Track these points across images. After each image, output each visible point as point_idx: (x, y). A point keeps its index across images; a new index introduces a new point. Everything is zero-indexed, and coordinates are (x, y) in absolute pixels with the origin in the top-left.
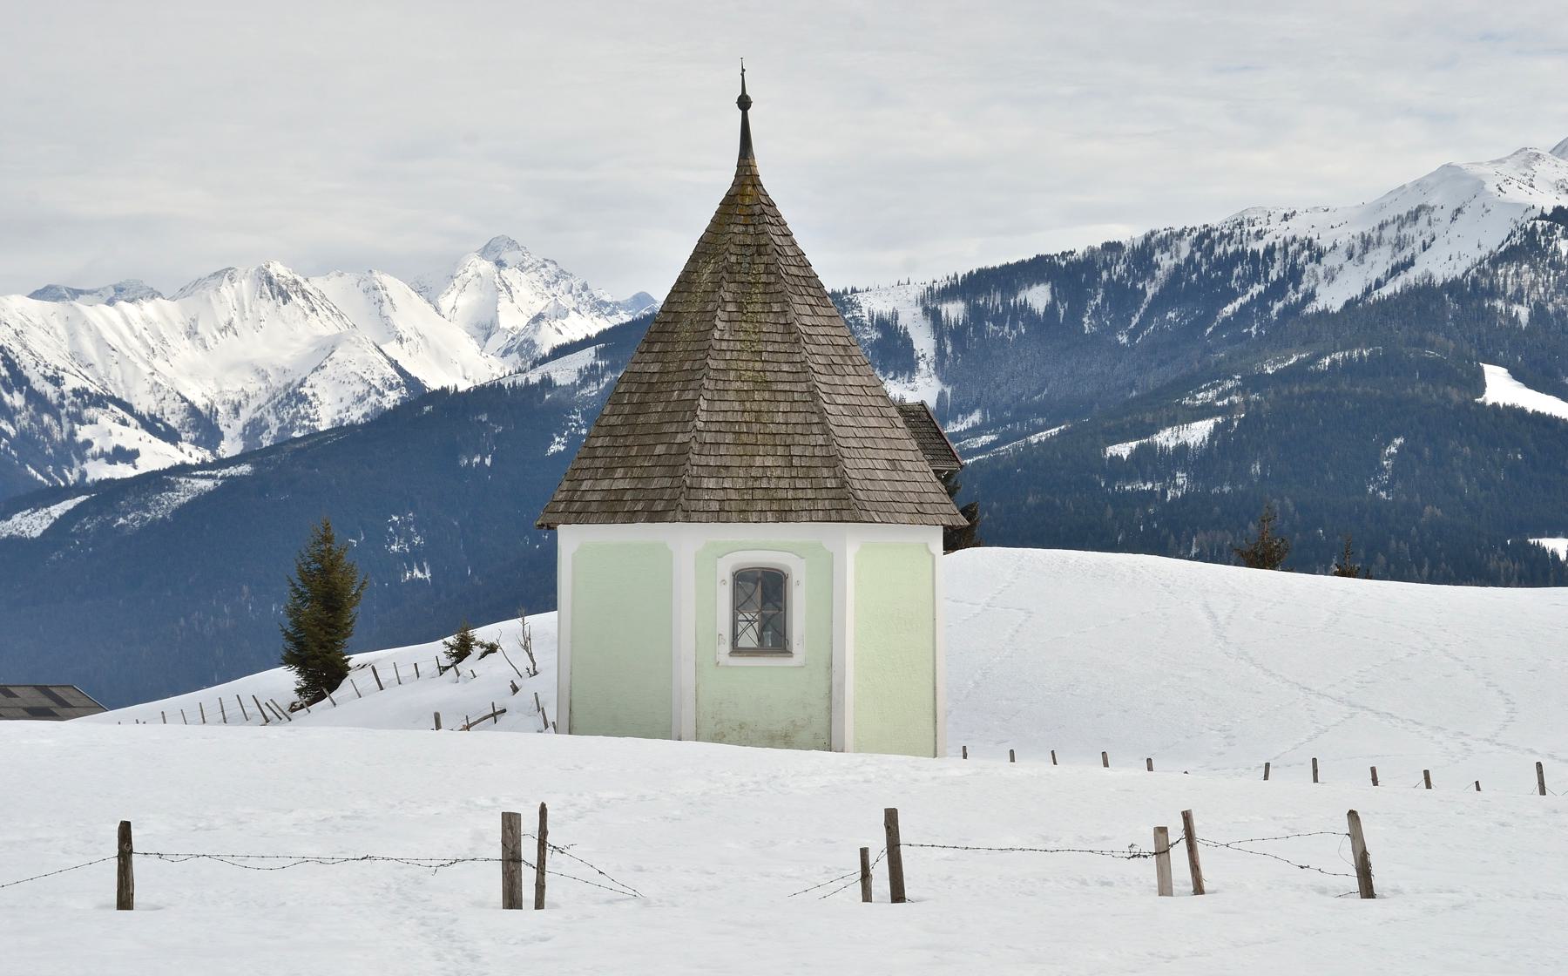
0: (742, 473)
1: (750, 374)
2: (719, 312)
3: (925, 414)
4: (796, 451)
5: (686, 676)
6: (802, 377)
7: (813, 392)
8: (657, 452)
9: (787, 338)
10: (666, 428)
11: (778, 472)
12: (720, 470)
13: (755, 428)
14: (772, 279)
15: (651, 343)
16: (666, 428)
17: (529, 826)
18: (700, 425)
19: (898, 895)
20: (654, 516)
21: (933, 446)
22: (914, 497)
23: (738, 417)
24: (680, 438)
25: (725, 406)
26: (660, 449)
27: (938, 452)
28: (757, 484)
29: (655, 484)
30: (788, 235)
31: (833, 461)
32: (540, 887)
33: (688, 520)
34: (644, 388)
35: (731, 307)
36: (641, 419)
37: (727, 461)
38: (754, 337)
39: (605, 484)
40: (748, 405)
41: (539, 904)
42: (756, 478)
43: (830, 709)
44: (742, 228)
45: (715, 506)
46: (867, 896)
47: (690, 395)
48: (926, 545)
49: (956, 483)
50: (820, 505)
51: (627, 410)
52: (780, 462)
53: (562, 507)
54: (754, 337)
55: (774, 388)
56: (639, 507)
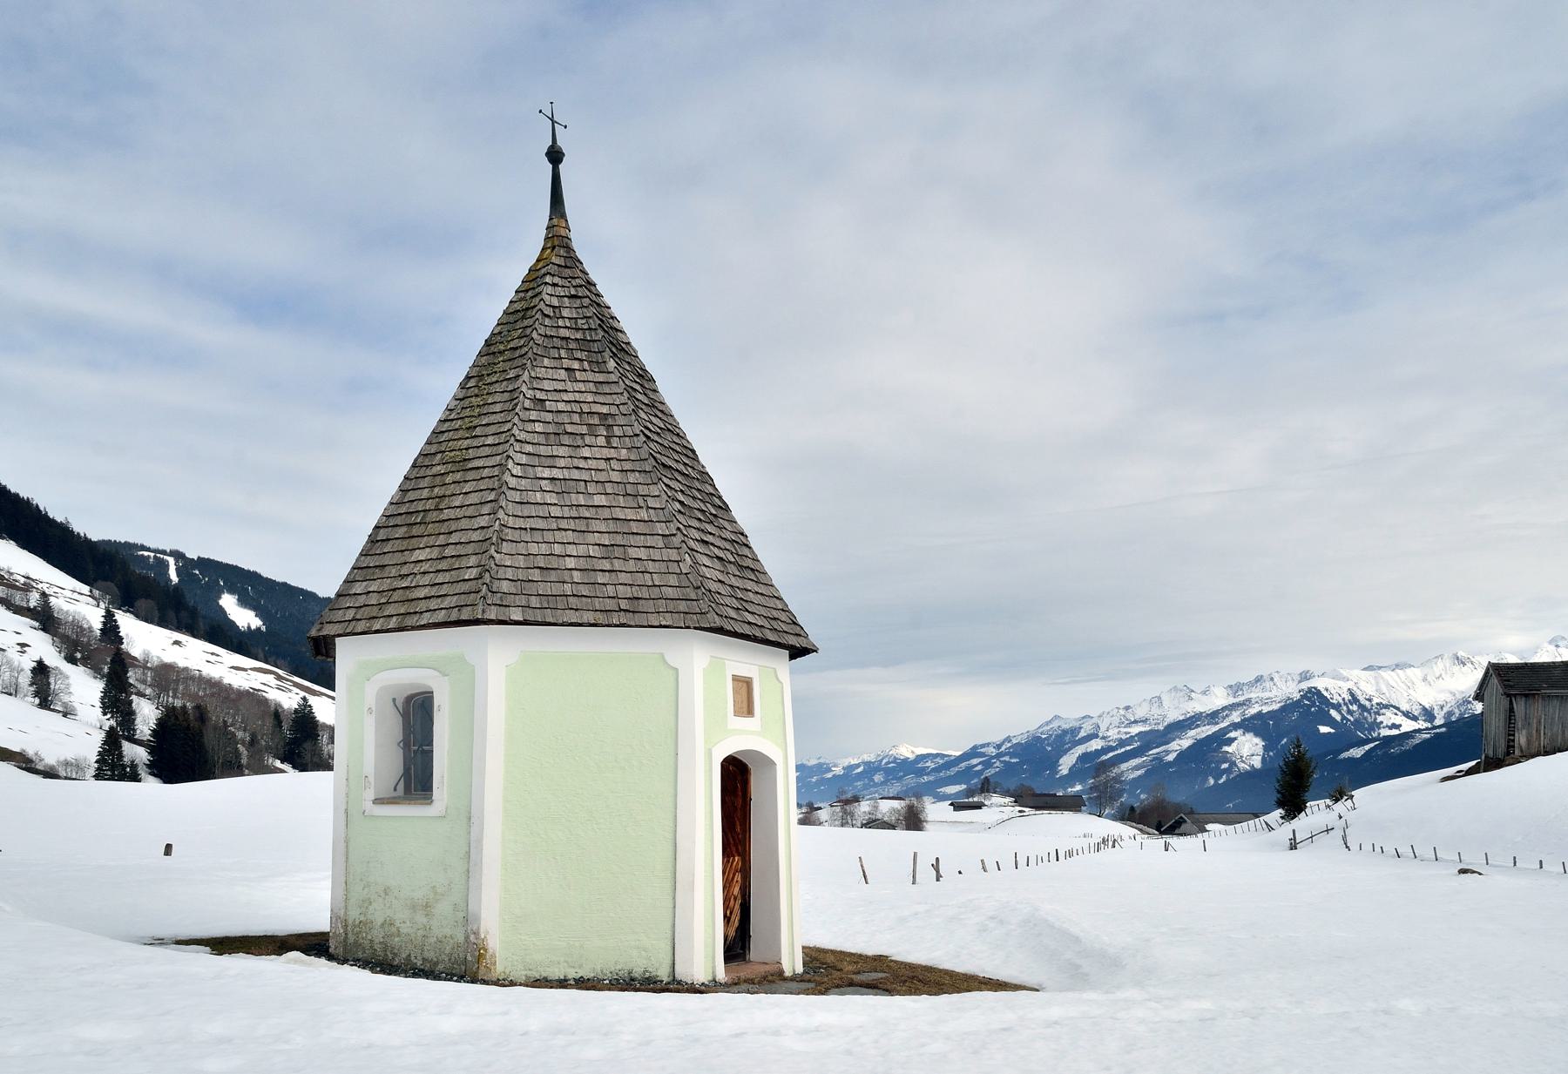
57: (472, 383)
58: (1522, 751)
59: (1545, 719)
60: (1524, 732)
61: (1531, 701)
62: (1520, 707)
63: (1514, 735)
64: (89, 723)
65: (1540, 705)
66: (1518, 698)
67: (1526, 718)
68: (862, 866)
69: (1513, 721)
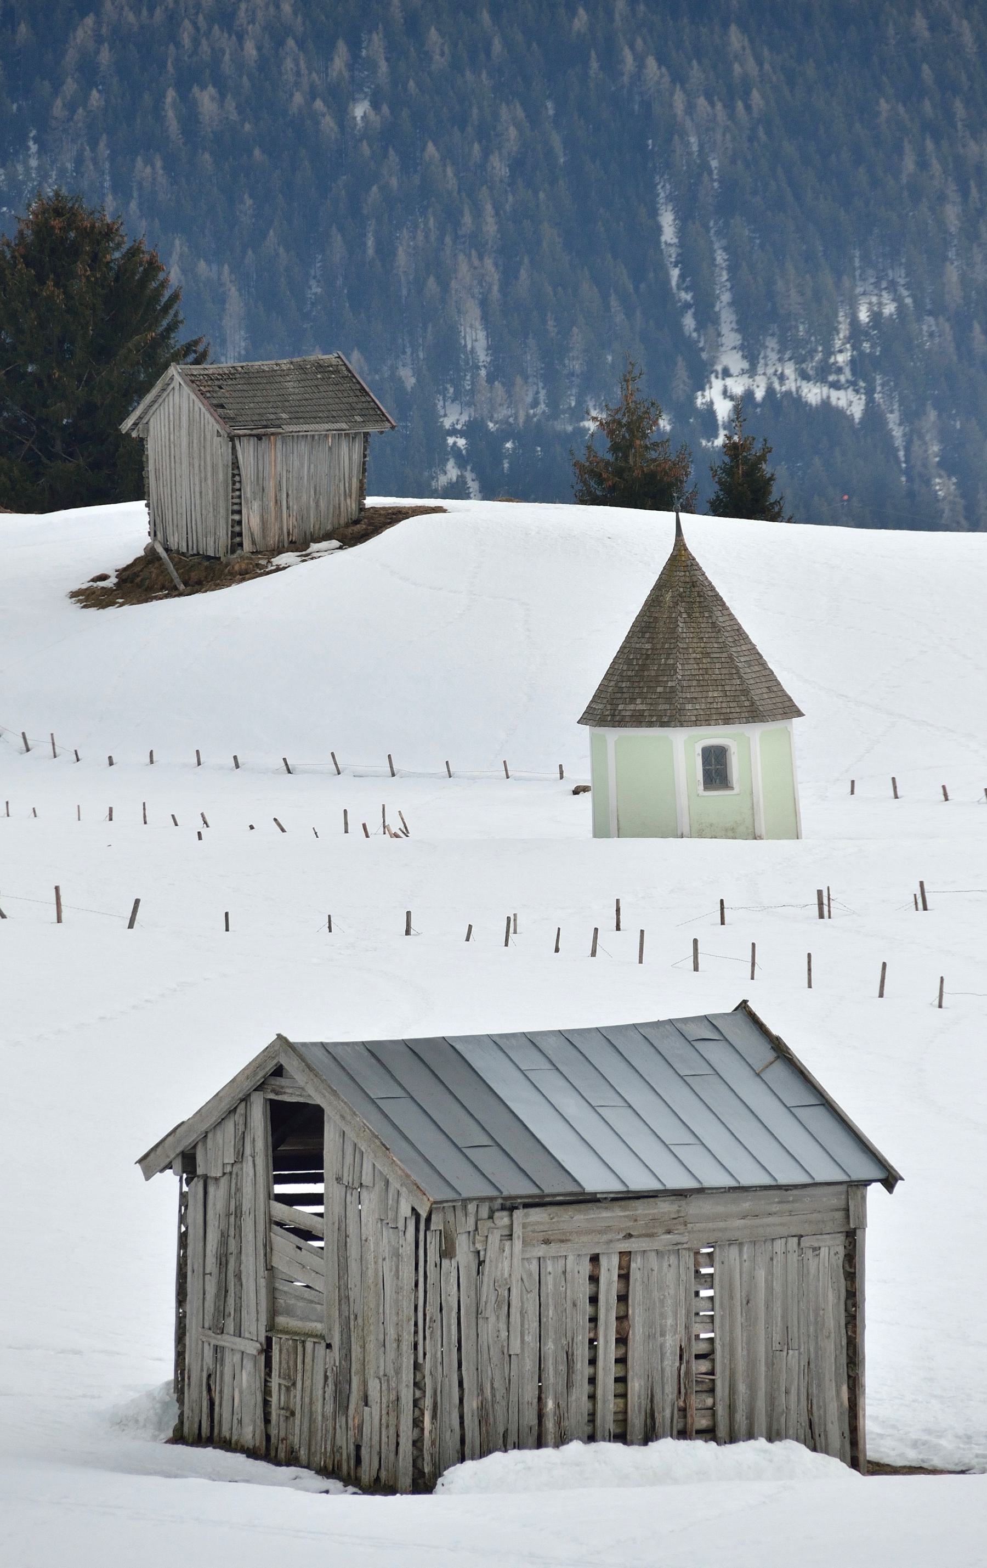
0: (703, 700)
1: (699, 649)
2: (679, 618)
3: (344, 368)
4: (727, 688)
5: (683, 801)
6: (724, 649)
7: (730, 657)
8: (658, 691)
9: (714, 629)
10: (661, 678)
11: (720, 700)
12: (692, 700)
13: (706, 677)
14: (702, 599)
15: (644, 633)
16: (661, 678)
17: (825, 894)
18: (680, 677)
19: (925, 908)
20: (663, 724)
21: (359, 406)
22: (780, 705)
23: (697, 672)
24: (670, 684)
25: (690, 667)
26: (660, 689)
27: (366, 412)
28: (712, 706)
29: (660, 707)
30: (703, 574)
31: (746, 692)
32: (829, 911)
33: (682, 726)
34: (644, 657)
35: (684, 615)
36: (646, 673)
37: (695, 695)
38: (698, 630)
39: (632, 707)
40: (701, 665)
41: (830, 917)
42: (711, 703)
43: (753, 814)
44: (683, 573)
45: (694, 718)
46: (917, 909)
47: (671, 662)
48: (786, 728)
49: (176, 315)
50: (743, 715)
51: (637, 668)
52: (721, 694)
53: (609, 718)
54: (698, 630)
55: (712, 656)
56: (654, 719)
57: (626, 651)
58: (254, 543)
59: (288, 479)
60: (256, 505)
61: (264, 443)
62: (247, 453)
63: (240, 512)
64: (591, 1418)
65: (279, 455)
66: (245, 440)
67: (259, 480)
68: (402, 819)
69: (237, 486)
